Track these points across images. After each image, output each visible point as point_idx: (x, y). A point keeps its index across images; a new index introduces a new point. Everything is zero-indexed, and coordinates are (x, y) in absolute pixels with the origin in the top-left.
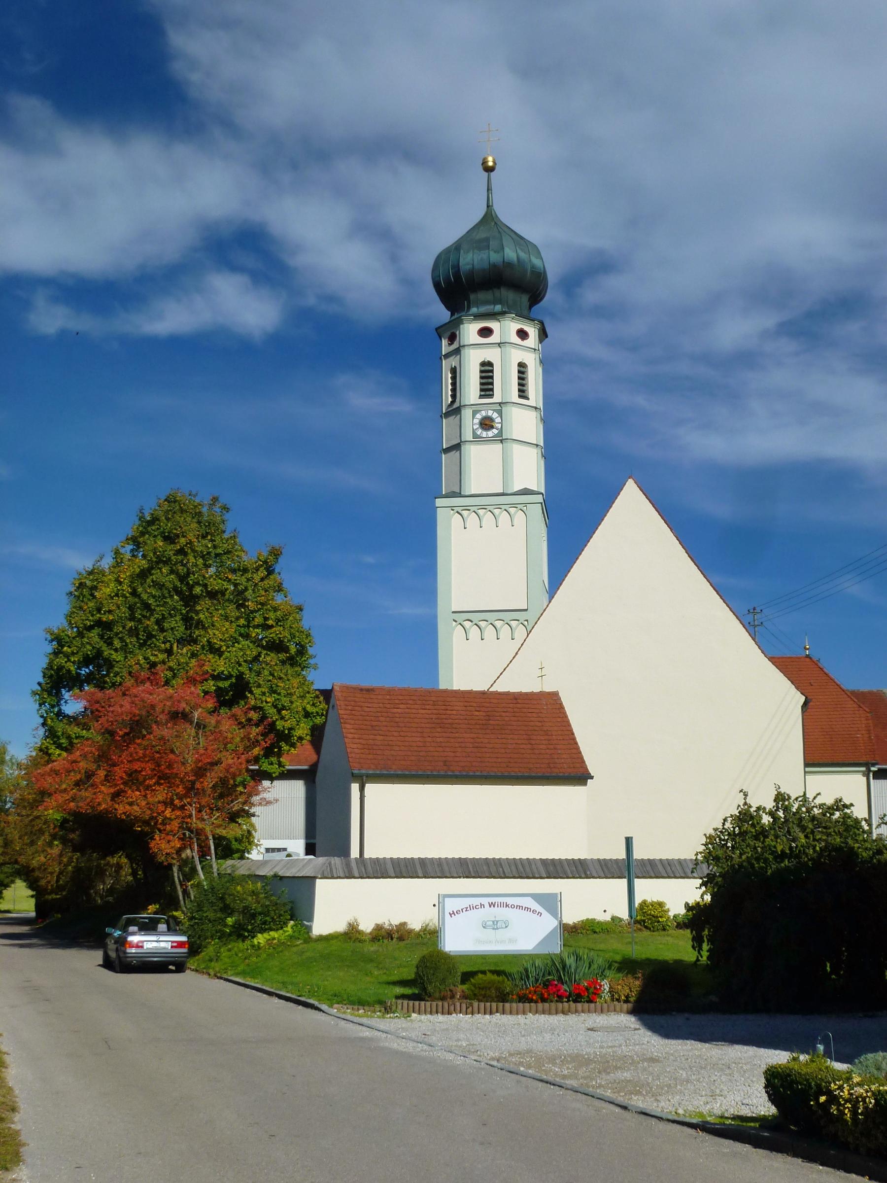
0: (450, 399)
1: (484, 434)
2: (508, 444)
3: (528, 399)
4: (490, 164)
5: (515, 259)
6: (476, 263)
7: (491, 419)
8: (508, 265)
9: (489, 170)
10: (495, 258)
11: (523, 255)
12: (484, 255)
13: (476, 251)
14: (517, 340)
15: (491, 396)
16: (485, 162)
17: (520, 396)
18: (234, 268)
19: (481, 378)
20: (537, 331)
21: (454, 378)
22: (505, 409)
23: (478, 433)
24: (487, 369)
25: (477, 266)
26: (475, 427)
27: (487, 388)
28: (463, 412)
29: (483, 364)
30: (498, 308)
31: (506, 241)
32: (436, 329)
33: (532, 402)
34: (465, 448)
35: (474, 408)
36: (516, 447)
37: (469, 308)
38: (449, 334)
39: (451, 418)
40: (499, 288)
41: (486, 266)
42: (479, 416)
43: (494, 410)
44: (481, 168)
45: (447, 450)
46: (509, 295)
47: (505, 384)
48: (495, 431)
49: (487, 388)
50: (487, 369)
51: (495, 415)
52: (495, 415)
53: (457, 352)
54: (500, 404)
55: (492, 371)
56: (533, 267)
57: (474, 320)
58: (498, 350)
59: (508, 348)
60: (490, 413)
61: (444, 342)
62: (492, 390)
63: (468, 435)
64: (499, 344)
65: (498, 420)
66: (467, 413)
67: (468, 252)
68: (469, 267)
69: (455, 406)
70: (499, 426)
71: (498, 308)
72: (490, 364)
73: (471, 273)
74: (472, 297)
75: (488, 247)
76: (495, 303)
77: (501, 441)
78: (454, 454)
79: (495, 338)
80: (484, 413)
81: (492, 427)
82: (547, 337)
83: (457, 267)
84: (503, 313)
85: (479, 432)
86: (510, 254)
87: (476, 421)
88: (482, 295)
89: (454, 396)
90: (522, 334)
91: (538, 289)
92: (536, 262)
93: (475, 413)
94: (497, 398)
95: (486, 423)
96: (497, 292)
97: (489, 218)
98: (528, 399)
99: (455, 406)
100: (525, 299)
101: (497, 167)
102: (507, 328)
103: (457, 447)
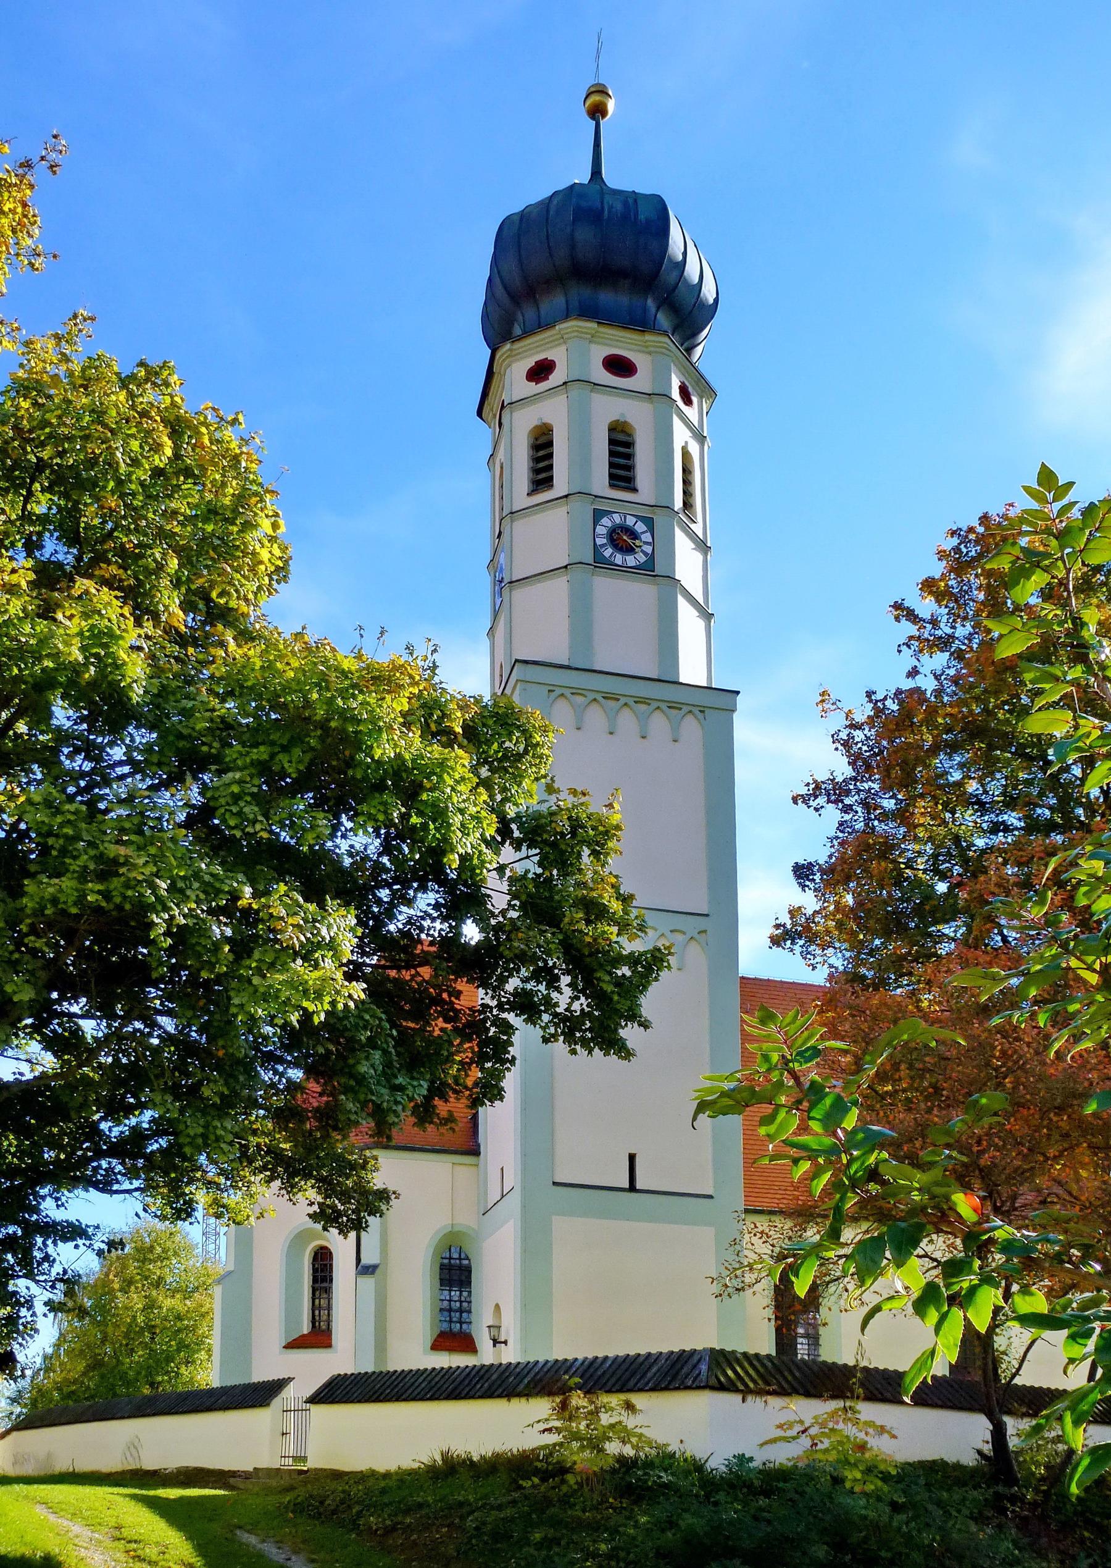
26: (599, 541)
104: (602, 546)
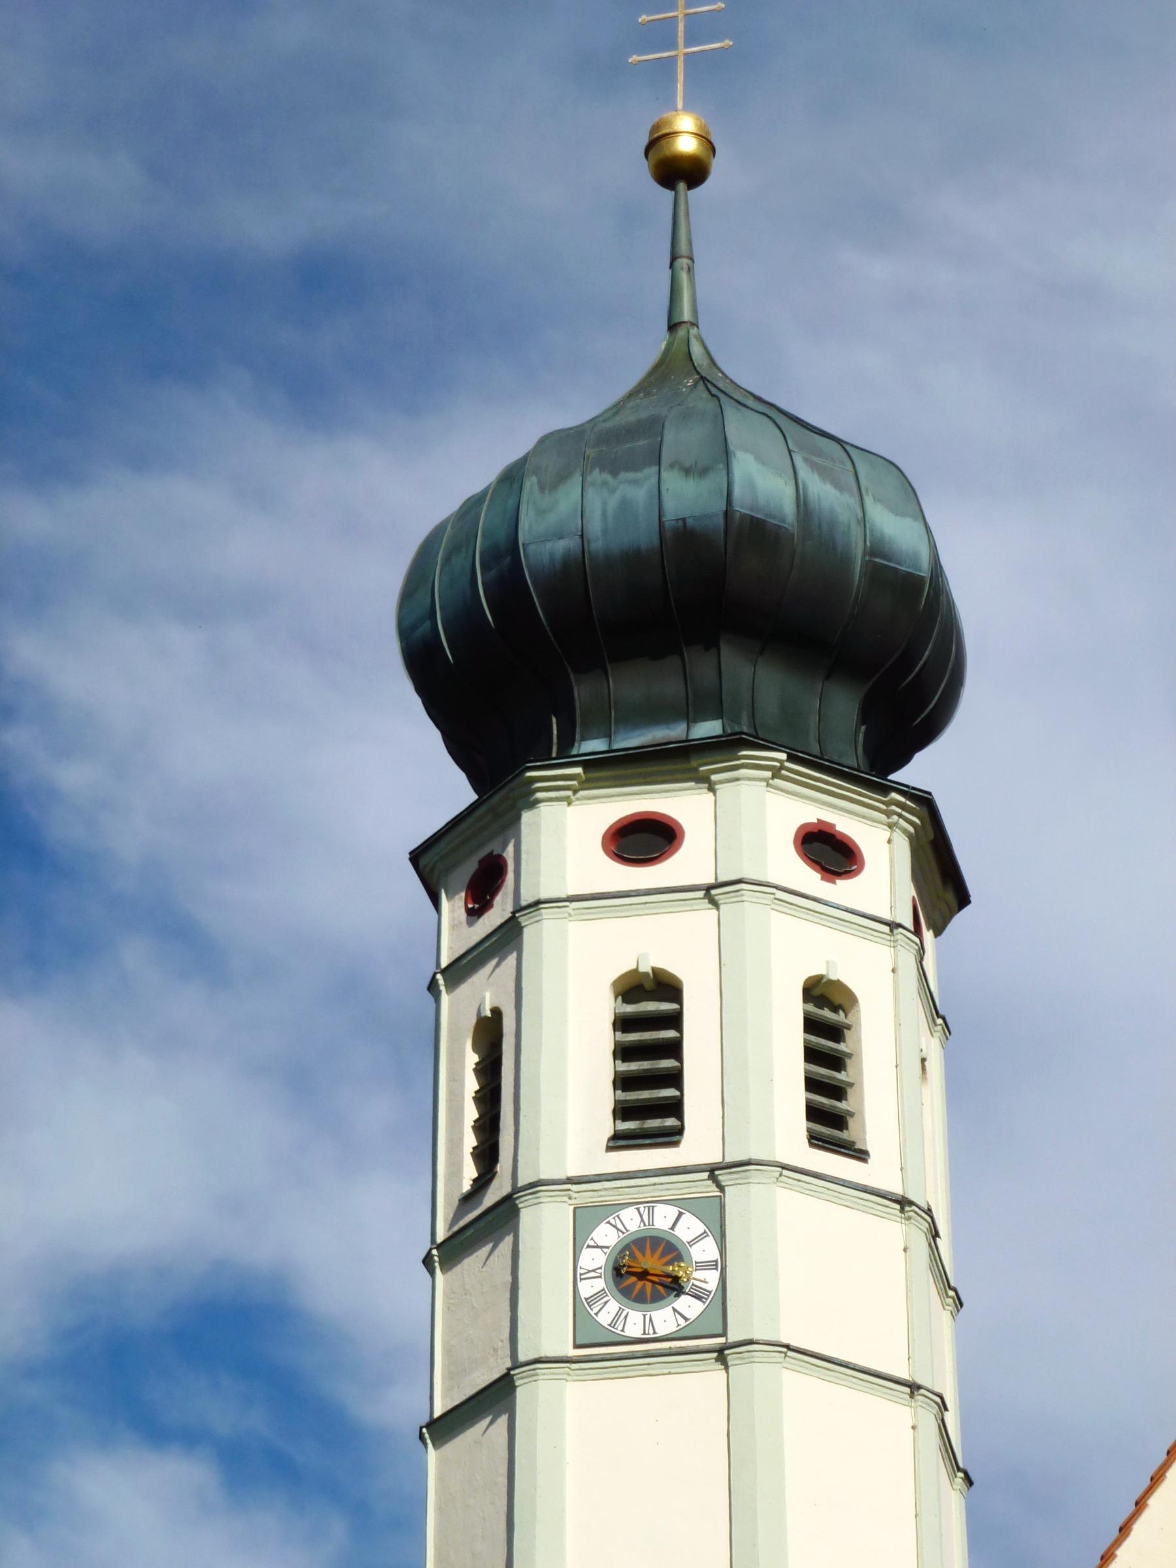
0: (470, 1171)
1: (634, 1323)
2: (756, 1371)
3: (861, 1155)
4: (686, 145)
5: (789, 509)
6: (595, 527)
7: (670, 1249)
8: (753, 533)
9: (680, 174)
10: (686, 497)
11: (821, 491)
12: (636, 489)
13: (596, 475)
14: (807, 878)
15: (672, 1137)
16: (658, 140)
17: (816, 1141)
18: (156, 1432)
19: (623, 1052)
20: (903, 847)
21: (489, 1070)
22: (743, 1198)
23: (604, 1319)
24: (649, 1018)
25: (597, 544)
26: (587, 1289)
27: (648, 1096)
28: (526, 1217)
29: (634, 987)
30: (709, 728)
31: (738, 426)
32: (416, 857)
33: (882, 1171)
34: (530, 1394)
35: (585, 1195)
36: (798, 1386)
37: (567, 741)
38: (470, 867)
39: (472, 1263)
40: (711, 644)
41: (644, 535)
42: (606, 1235)
43: (684, 1205)
44: (643, 171)
45: (442, 1428)
46: (766, 683)
47: (742, 1077)
48: (689, 1307)
49: (648, 1096)
50: (649, 1018)
51: (689, 1228)
52: (689, 1228)
53: (508, 937)
54: (712, 1171)
55: (675, 1020)
56: (877, 550)
57: (587, 784)
58: (701, 919)
59: (749, 910)
60: (663, 1217)
61: (453, 907)
62: (675, 1108)
63: (549, 1329)
64: (708, 889)
65: (706, 1250)
66: (545, 1225)
67: (562, 478)
68: (560, 547)
69: (491, 1197)
70: (711, 1280)
71: (709, 728)
72: (666, 987)
73: (576, 575)
74: (582, 692)
75: (656, 457)
76: (692, 713)
77: (721, 1355)
78: (485, 1435)
79: (686, 865)
80: (631, 1220)
81: (675, 1286)
82: (963, 899)
83: (506, 556)
84: (726, 747)
85: (608, 1312)
86: (764, 481)
87: (594, 1259)
88: (627, 684)
89: (487, 1155)
90: (828, 852)
91: (908, 658)
92: (895, 529)
93: (584, 1221)
94: (700, 1141)
95: (646, 1272)
96: (702, 666)
97: (683, 372)
98: (861, 1155)
99: (491, 1197)
100: (841, 710)
101: (717, 168)
102: (746, 816)
103: (496, 1397)
104: (591, 1300)
